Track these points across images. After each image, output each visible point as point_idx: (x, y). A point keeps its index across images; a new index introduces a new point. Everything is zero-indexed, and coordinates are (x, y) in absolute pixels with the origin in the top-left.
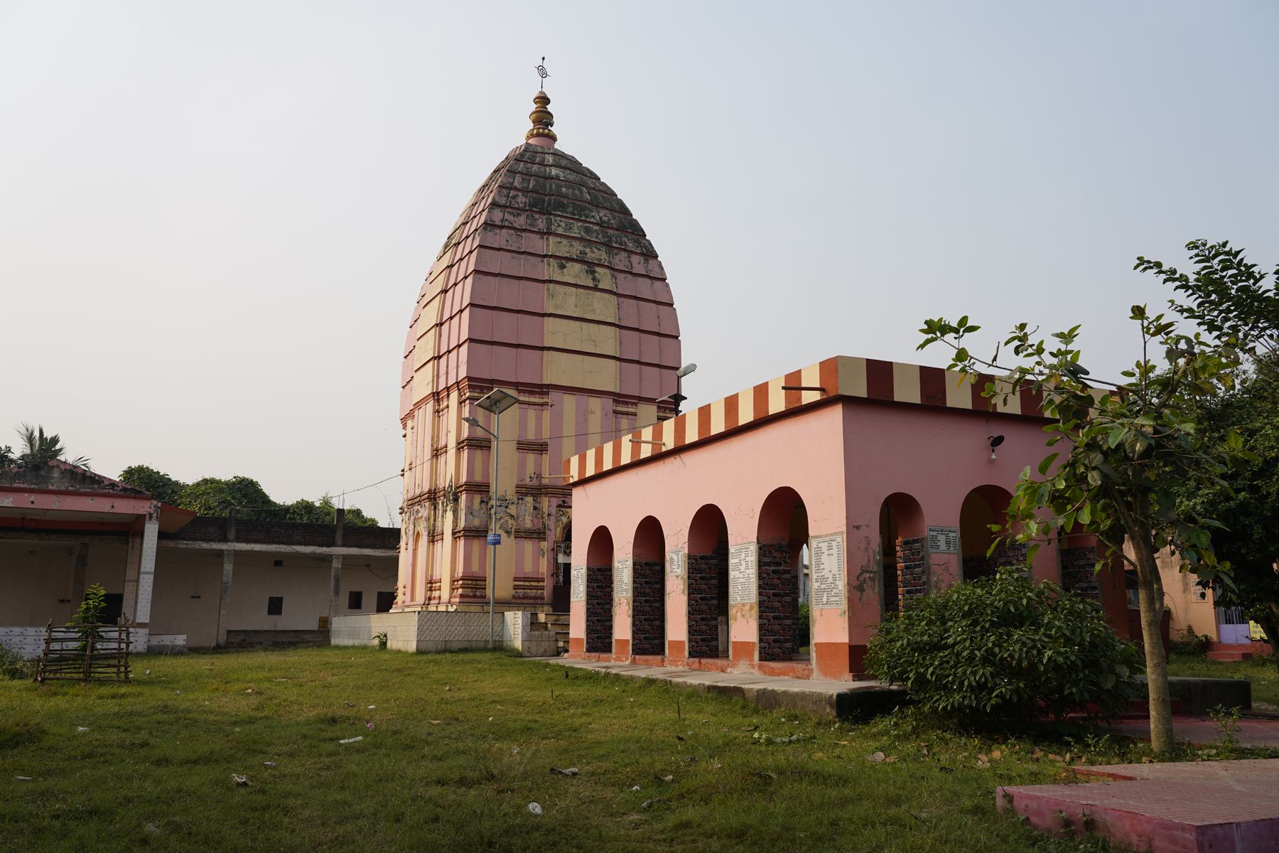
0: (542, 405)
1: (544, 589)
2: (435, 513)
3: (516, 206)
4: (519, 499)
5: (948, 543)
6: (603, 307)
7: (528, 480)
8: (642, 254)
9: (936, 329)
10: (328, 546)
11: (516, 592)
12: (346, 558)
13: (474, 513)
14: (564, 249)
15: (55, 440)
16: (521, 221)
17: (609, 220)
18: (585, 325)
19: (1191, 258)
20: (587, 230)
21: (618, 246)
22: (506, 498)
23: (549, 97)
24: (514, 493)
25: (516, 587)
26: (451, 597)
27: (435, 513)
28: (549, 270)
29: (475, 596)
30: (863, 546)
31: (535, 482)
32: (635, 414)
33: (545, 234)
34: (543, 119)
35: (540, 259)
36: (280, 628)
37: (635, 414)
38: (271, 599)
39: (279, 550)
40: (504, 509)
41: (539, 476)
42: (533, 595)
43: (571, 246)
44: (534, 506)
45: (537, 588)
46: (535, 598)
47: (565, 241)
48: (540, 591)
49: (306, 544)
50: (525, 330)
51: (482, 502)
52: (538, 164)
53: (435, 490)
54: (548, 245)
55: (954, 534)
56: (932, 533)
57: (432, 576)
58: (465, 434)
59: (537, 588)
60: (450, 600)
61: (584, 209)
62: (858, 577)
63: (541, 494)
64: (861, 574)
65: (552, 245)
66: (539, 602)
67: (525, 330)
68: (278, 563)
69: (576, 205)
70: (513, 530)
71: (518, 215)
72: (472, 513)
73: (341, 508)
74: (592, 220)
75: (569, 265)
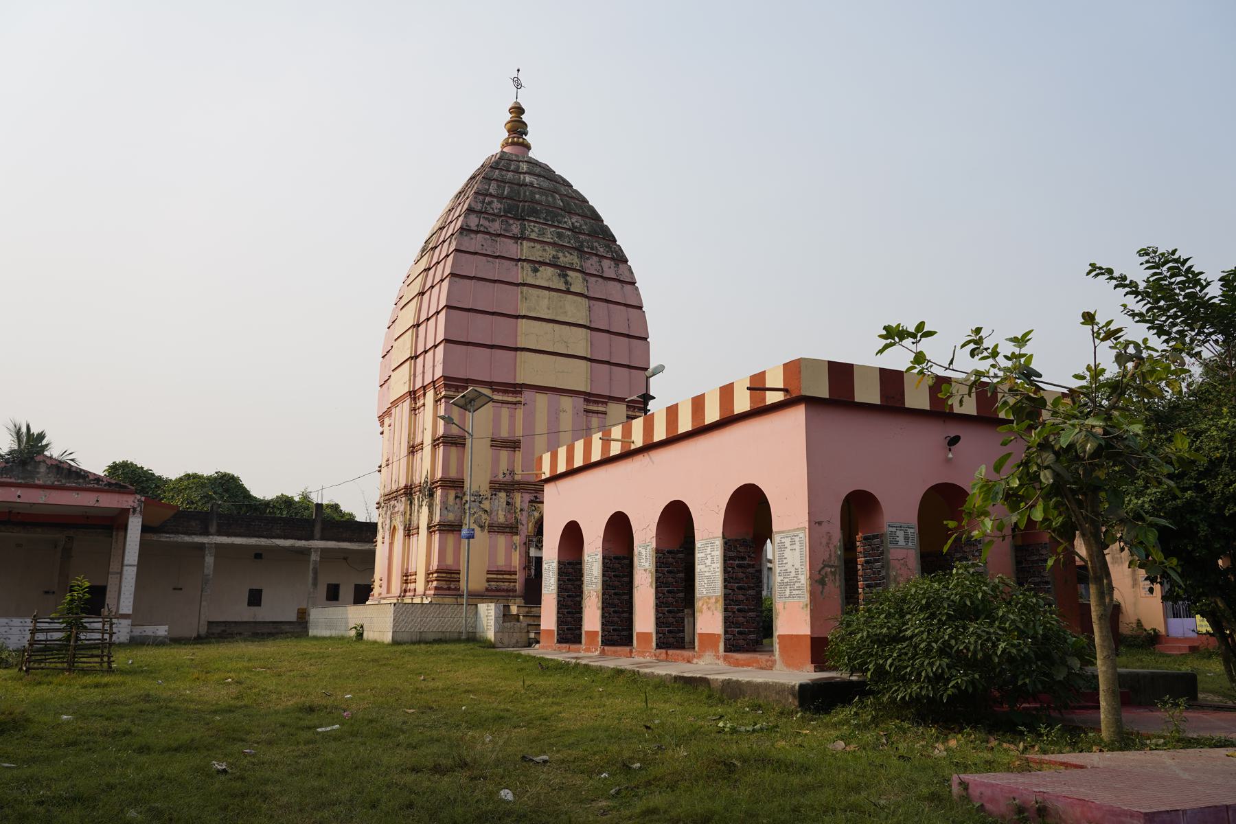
0: (515, 404)
1: (516, 582)
2: (411, 507)
3: (491, 211)
4: (492, 495)
5: (906, 539)
6: (575, 309)
7: (501, 476)
8: (612, 259)
9: (894, 334)
10: (307, 539)
11: (489, 585)
12: (324, 551)
13: (448, 508)
14: (537, 253)
15: (41, 436)
16: (496, 226)
17: (581, 226)
18: (557, 326)
19: (1142, 264)
20: (560, 236)
21: (589, 250)
22: (480, 493)
23: (523, 106)
24: (488, 490)
25: (489, 580)
26: (425, 590)
27: (411, 507)
28: (524, 274)
29: (449, 589)
30: (824, 541)
31: (508, 478)
32: (605, 413)
33: (519, 238)
34: (517, 127)
35: (514, 263)
36: (259, 619)
37: (605, 413)
38: (251, 591)
39: (259, 543)
40: (477, 504)
41: (512, 473)
42: (505, 588)
43: (544, 250)
44: (508, 502)
45: (509, 581)
46: (508, 591)
47: (538, 246)
48: (512, 584)
49: (286, 537)
50: (499, 331)
51: (456, 497)
52: (512, 171)
53: (411, 485)
54: (522, 250)
55: (912, 531)
56: (891, 529)
57: (407, 569)
58: (441, 432)
59: (509, 581)
60: (425, 593)
61: (556, 215)
62: (820, 571)
63: (513, 490)
64: (823, 568)
65: (526, 250)
66: (511, 594)
67: (499, 331)
68: (258, 556)
69: (550, 211)
70: (486, 525)
71: (493, 220)
72: (446, 508)
73: (320, 503)
74: (565, 226)
75: (542, 268)
